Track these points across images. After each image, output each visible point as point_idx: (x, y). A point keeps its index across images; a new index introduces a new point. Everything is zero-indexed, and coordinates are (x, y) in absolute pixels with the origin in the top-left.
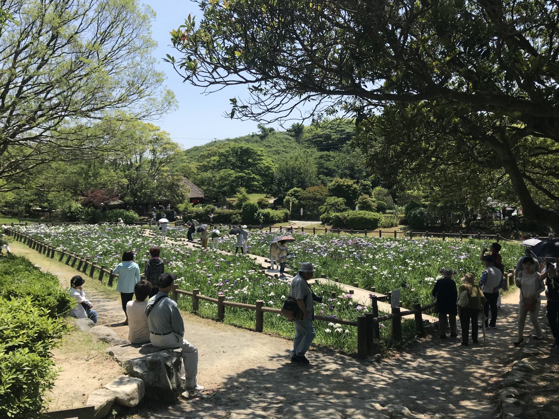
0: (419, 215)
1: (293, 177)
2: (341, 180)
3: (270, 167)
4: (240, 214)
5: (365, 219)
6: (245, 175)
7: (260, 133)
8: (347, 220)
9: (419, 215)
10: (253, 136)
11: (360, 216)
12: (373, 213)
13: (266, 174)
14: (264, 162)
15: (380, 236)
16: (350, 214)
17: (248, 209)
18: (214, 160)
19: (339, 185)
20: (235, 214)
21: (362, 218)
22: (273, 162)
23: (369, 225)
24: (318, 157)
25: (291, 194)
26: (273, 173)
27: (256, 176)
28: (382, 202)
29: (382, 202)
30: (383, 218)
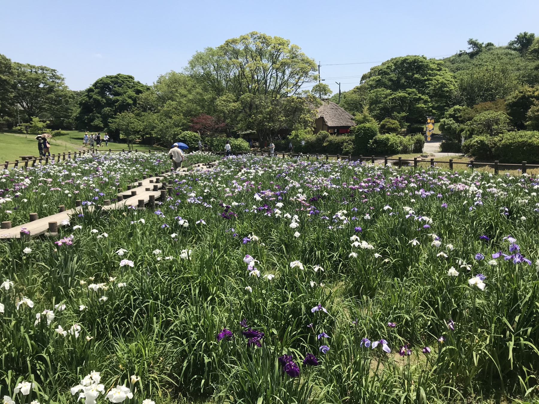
1: (476, 93)
2: (530, 89)
3: (445, 84)
5: (530, 145)
6: (407, 95)
7: (471, 50)
8: (498, 147)
10: (460, 55)
11: (520, 140)
18: (374, 80)
19: (524, 97)
20: (347, 142)
21: (524, 144)
24: (532, 68)
26: (450, 92)
27: (423, 97)
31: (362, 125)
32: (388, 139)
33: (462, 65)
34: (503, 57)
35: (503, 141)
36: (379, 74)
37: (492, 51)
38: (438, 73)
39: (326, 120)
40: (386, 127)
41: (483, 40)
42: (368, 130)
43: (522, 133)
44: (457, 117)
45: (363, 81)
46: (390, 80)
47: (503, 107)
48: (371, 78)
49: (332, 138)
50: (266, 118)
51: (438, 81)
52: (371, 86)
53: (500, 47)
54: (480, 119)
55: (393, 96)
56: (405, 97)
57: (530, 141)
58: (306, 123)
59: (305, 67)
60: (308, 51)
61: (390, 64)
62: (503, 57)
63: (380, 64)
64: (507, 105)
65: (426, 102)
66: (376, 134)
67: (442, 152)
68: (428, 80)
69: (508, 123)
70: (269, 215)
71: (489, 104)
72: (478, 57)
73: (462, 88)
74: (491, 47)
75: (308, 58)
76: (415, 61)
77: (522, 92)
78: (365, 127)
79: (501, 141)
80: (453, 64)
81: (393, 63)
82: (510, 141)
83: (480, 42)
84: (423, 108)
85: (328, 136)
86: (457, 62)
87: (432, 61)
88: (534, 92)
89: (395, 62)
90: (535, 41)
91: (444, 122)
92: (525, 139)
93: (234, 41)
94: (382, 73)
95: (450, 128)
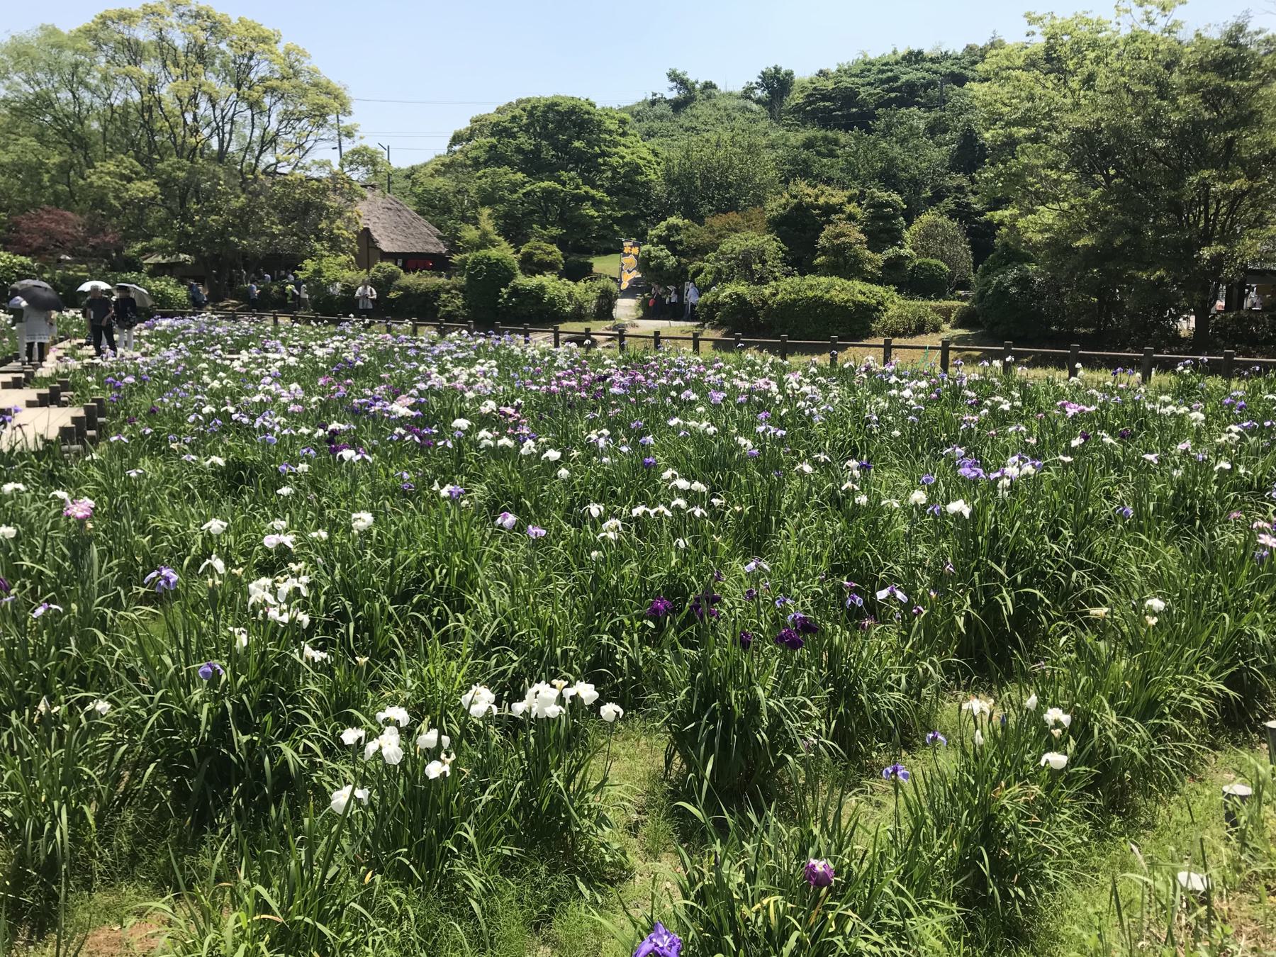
0: (1013, 290)
1: (708, 192)
2: (809, 191)
3: (638, 166)
4: (461, 289)
5: (828, 304)
8: (770, 307)
9: (1013, 290)
10: (653, 103)
11: (810, 294)
12: (858, 285)
13: (628, 186)
14: (621, 150)
15: (886, 360)
16: (788, 287)
17: (479, 273)
19: (799, 206)
20: (448, 292)
21: (818, 302)
22: (656, 155)
23: (853, 324)
25: (659, 237)
26: (646, 184)
27: (593, 192)
28: (934, 261)
29: (934, 261)
30: (897, 306)
31: (483, 252)
32: (542, 288)
33: (656, 125)
34: (737, 115)
35: (779, 297)
36: (492, 135)
37: (714, 101)
38: (622, 140)
39: (375, 235)
40: (535, 259)
41: (697, 76)
42: (496, 264)
43: (810, 279)
44: (674, 242)
45: (457, 148)
46: (519, 150)
47: (762, 224)
48: (473, 143)
49: (409, 279)
50: (233, 226)
51: (622, 157)
52: (476, 159)
53: (730, 94)
54: (733, 250)
55: (528, 188)
56: (554, 191)
57: (828, 296)
58: (335, 244)
59: (323, 105)
60: (326, 63)
61: (517, 112)
62: (737, 115)
63: (492, 110)
64: (769, 221)
65: (597, 204)
66: (512, 276)
67: (644, 317)
68: (603, 154)
69: (783, 260)
70: (449, 445)
71: (733, 217)
72: (688, 110)
73: (670, 179)
74: (713, 91)
75: (329, 82)
76: (572, 111)
77: (795, 197)
78: (489, 259)
79: (774, 295)
80: (639, 121)
81: (524, 110)
82: (793, 296)
83: (691, 77)
84: (592, 217)
85: (398, 277)
86: (648, 115)
87: (608, 113)
88: (817, 197)
89: (529, 108)
90: (796, 88)
91: (649, 252)
92: (819, 293)
93: (124, 17)
94: (500, 132)
95: (660, 266)
